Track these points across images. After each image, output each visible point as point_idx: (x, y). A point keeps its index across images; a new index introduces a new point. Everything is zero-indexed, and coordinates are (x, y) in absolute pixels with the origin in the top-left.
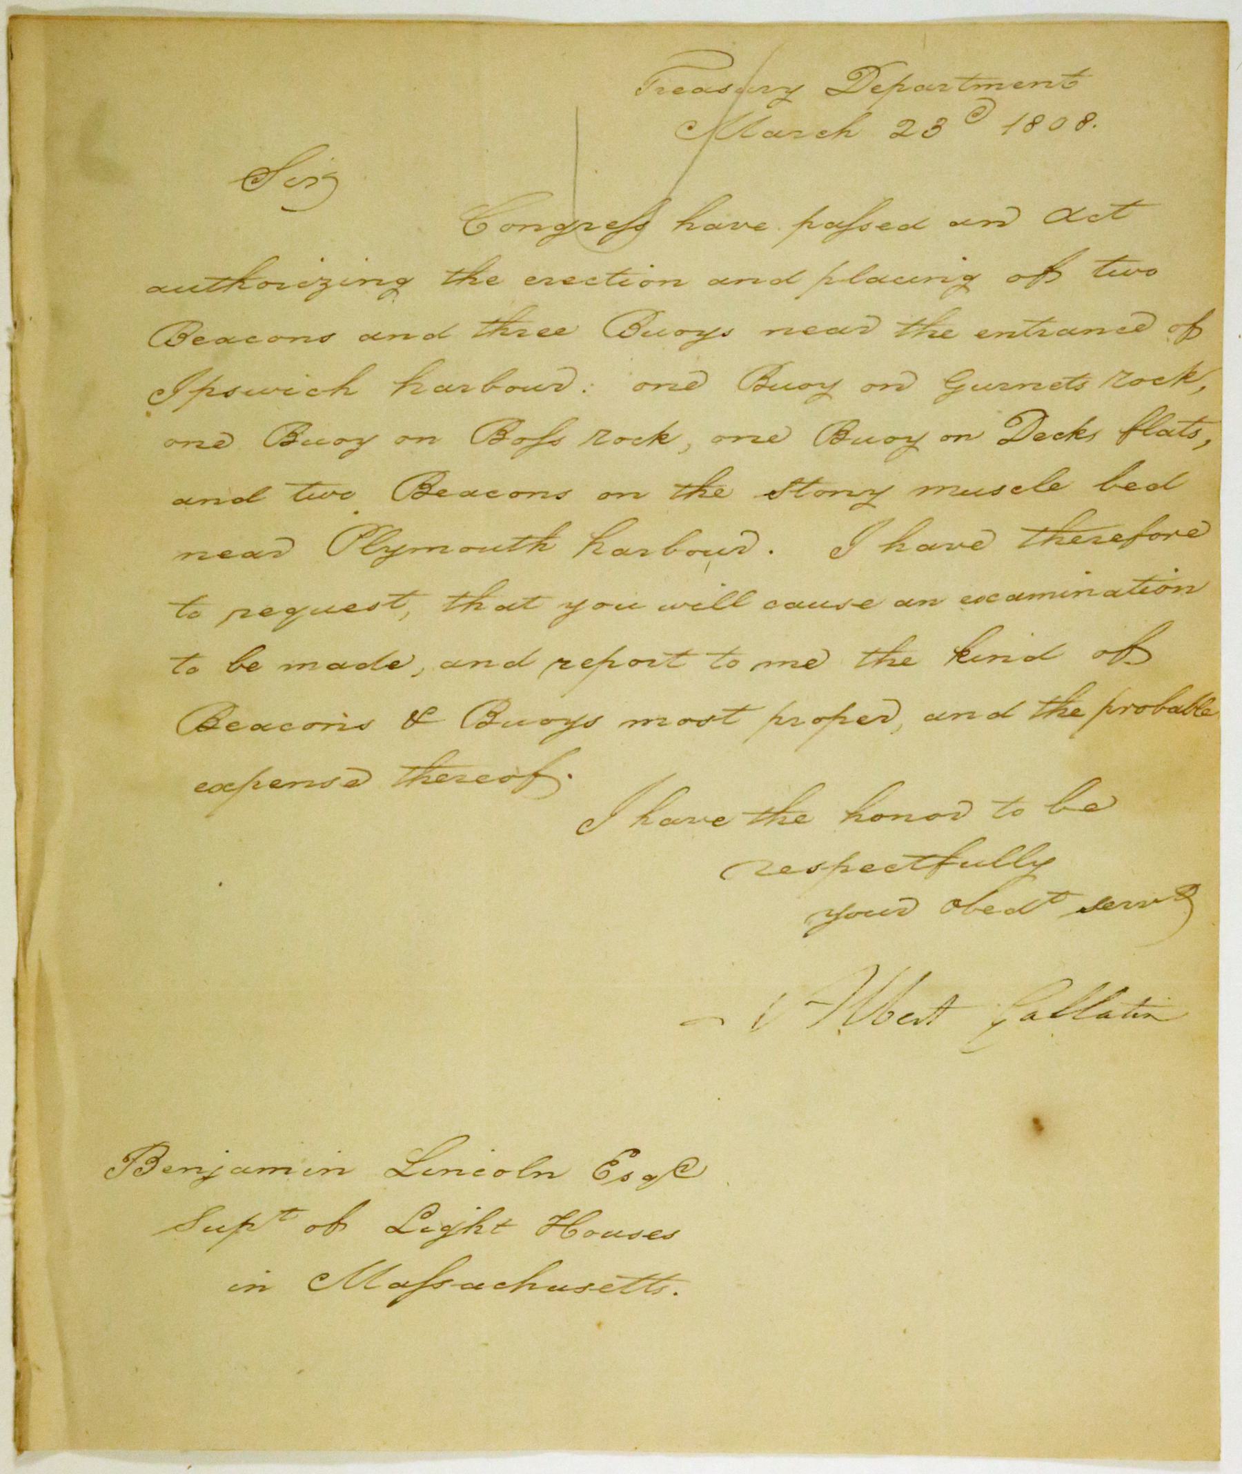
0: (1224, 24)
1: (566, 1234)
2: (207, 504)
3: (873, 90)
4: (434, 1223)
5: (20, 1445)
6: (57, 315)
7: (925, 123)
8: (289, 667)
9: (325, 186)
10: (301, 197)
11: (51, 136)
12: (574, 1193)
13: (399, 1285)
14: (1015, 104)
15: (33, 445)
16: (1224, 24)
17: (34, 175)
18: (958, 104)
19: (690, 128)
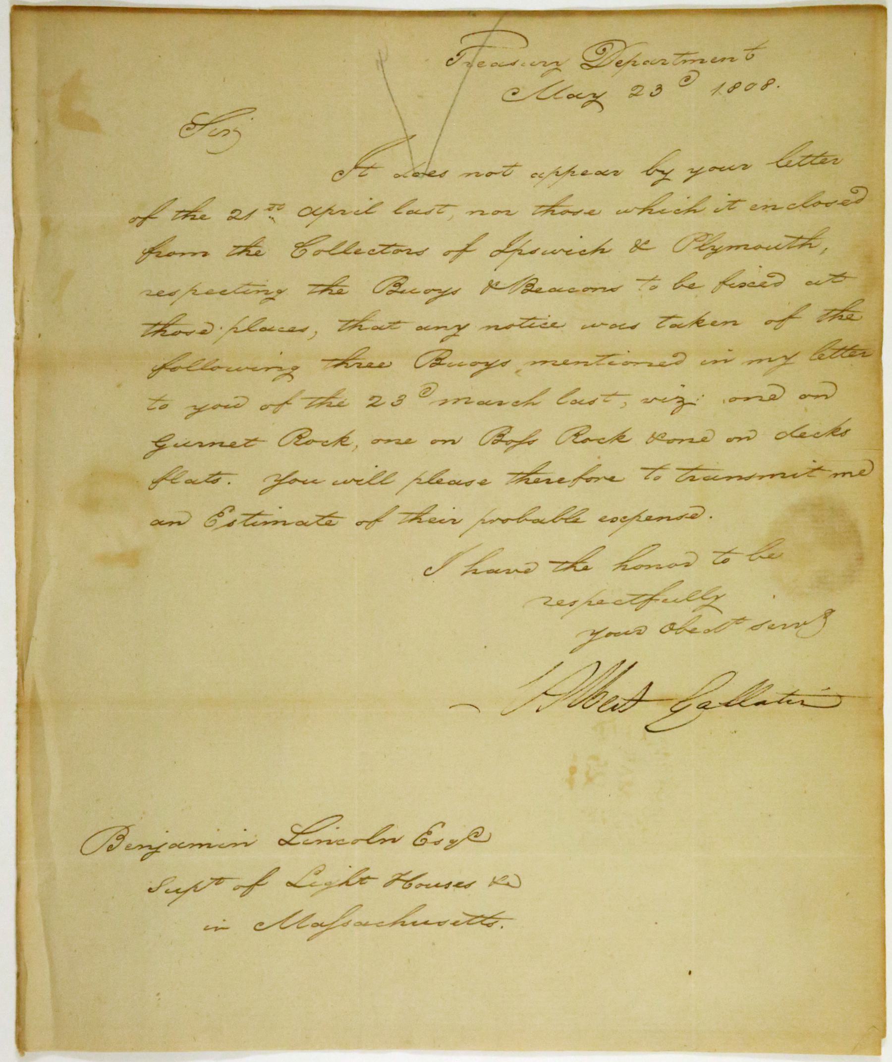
0: (16, 8)
1: (406, 886)
2: (763, 362)
3: (617, 64)
4: (321, 879)
5: (21, 1044)
6: (46, 225)
7: (651, 87)
8: (314, 482)
9: (233, 136)
10: (220, 143)
11: (43, 94)
12: (405, 858)
13: (318, 924)
14: (710, 75)
15: (27, 318)
16: (16, 8)
17: (30, 126)
18: (671, 75)
19: (514, 94)
